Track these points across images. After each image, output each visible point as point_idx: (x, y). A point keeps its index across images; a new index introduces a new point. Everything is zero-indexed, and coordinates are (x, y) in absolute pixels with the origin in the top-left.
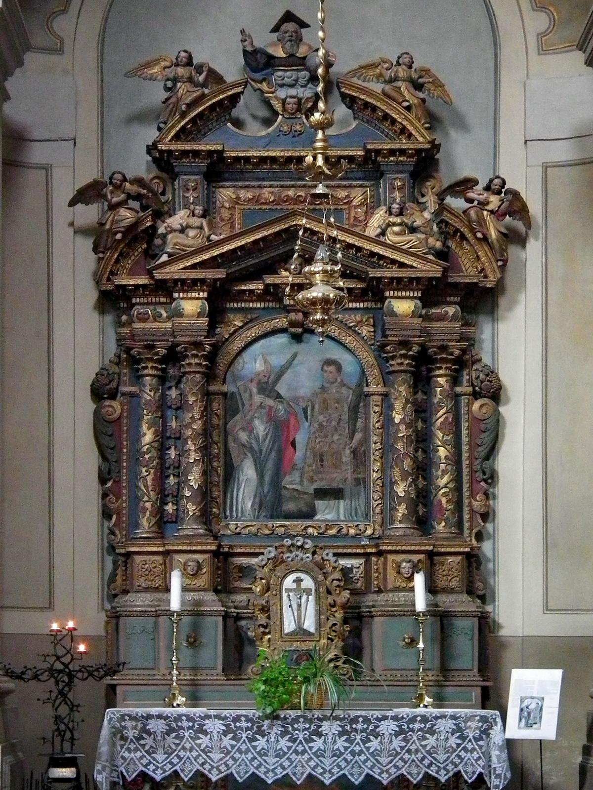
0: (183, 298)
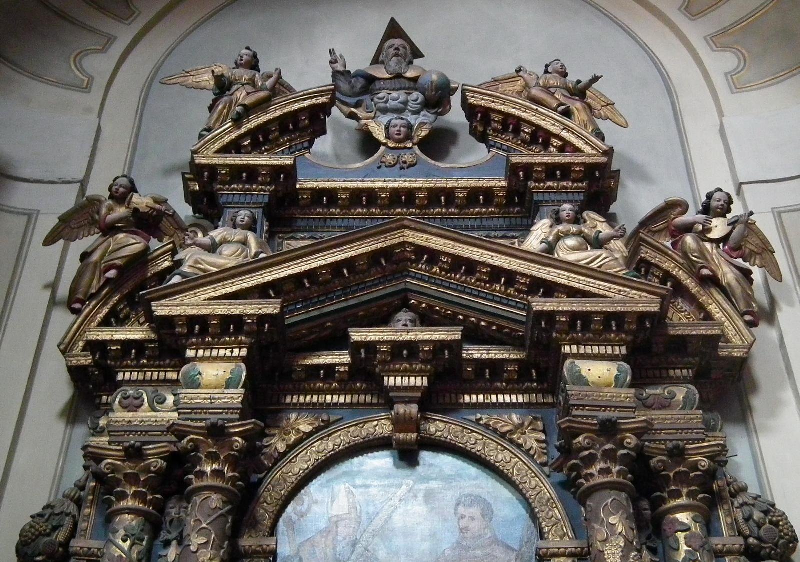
0: (203, 359)
